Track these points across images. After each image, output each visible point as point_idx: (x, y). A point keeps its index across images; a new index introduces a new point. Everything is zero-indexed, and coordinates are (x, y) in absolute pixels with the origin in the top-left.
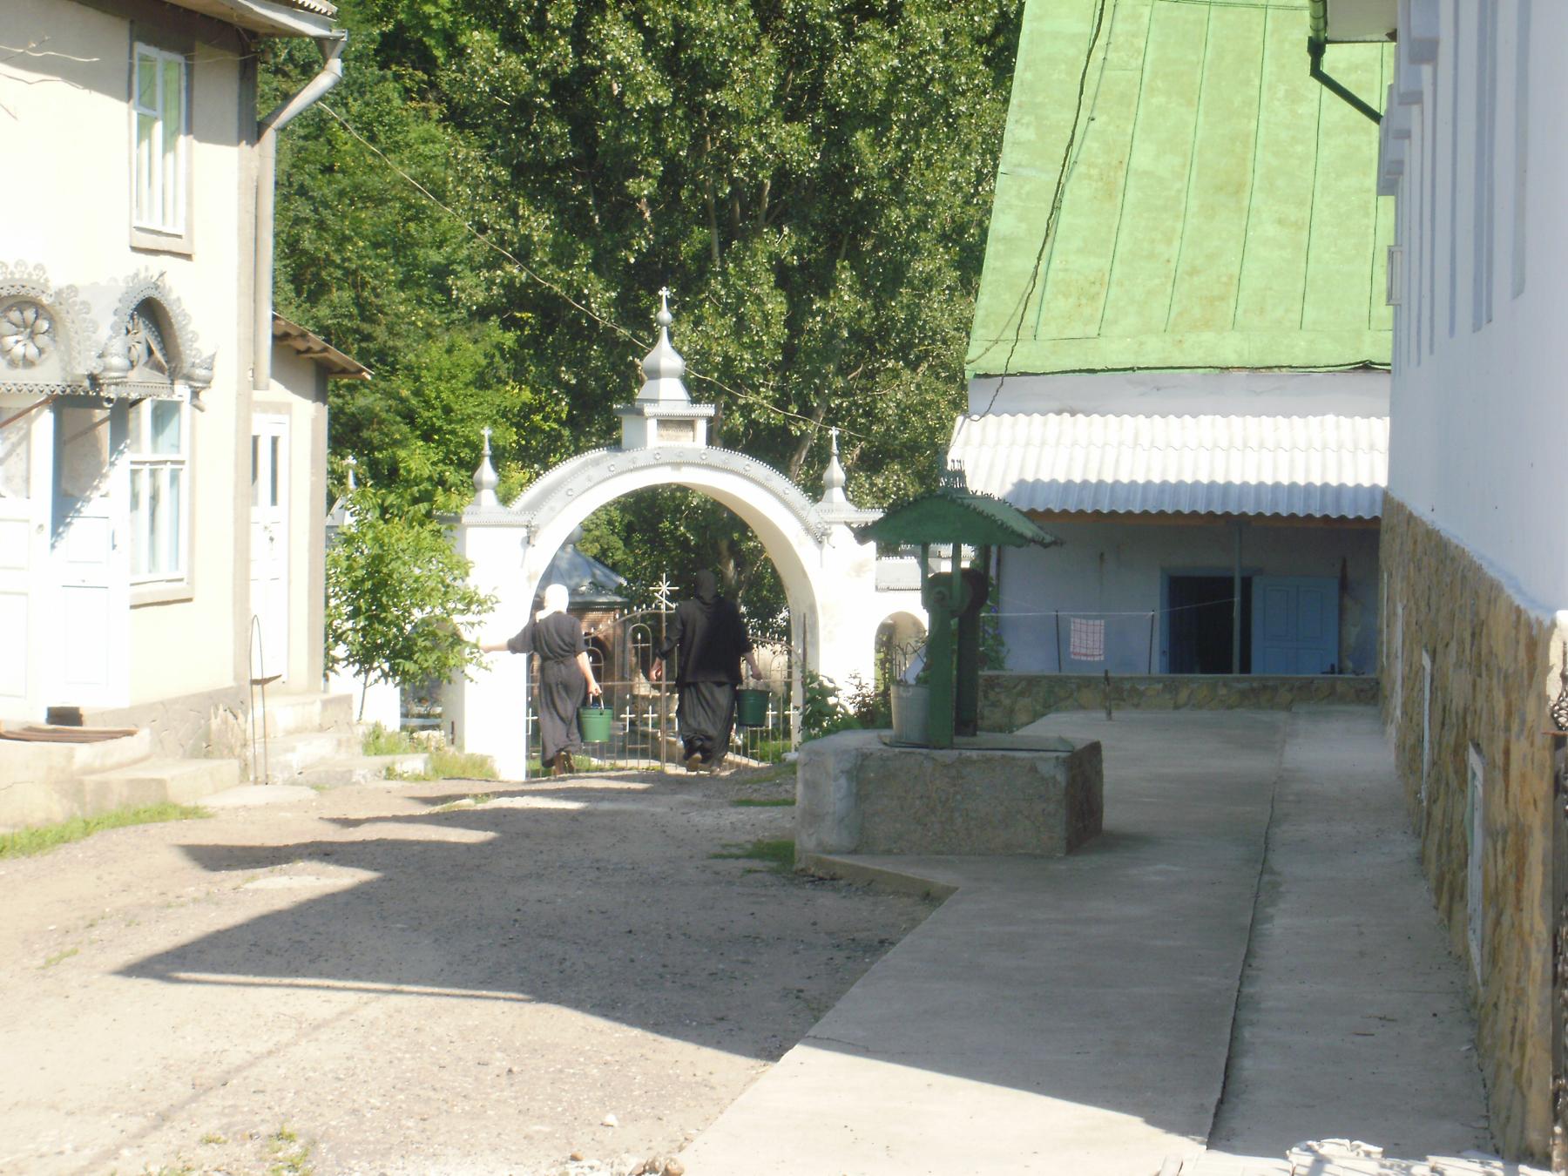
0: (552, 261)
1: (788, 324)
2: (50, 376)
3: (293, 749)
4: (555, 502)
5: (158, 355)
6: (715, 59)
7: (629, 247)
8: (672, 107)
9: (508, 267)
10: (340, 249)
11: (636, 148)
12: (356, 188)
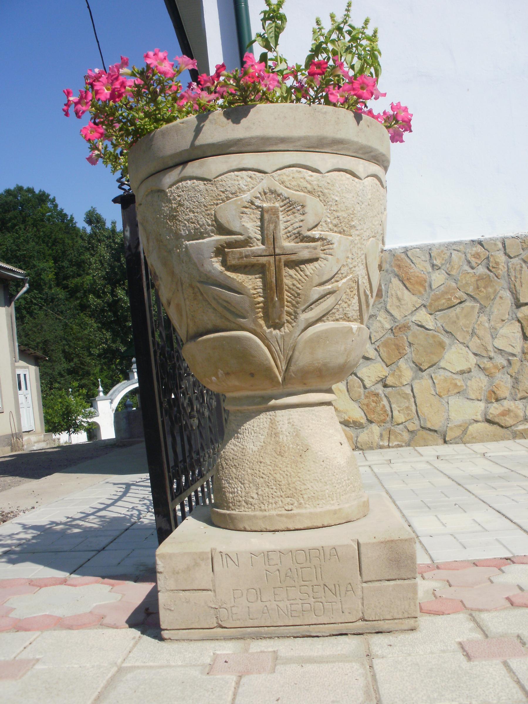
3: (34, 446)
7: (128, 337)
10: (74, 350)
12: (76, 337)
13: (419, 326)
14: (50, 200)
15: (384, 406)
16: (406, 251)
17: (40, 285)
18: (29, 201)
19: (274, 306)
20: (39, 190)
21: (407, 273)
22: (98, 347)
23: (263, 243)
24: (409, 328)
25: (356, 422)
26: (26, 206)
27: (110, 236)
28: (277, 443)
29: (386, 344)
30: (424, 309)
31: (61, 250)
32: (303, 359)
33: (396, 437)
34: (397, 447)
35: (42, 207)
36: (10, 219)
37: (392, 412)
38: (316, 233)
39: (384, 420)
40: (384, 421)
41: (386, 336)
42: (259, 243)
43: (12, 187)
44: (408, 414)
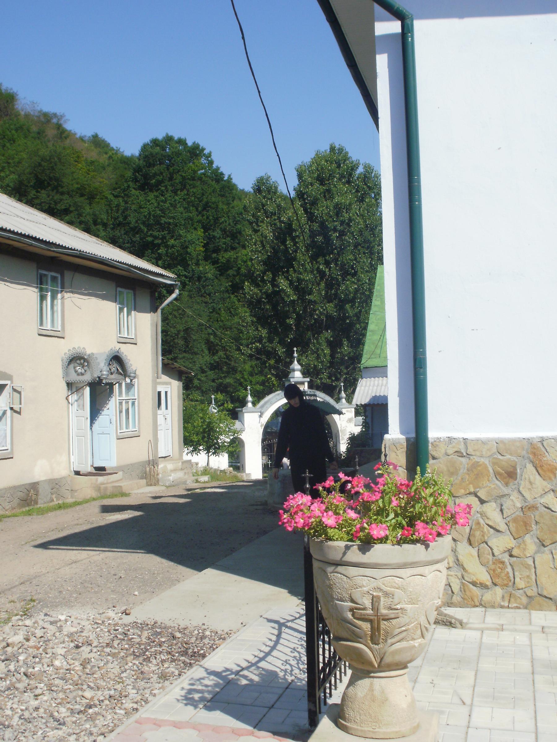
0: (268, 342)
1: (330, 356)
2: (88, 378)
3: (171, 476)
4: (267, 405)
5: (120, 371)
6: (308, 287)
7: (288, 337)
8: (297, 300)
9: (256, 344)
10: (220, 341)
11: (288, 311)
12: (224, 325)
13: (546, 507)
14: (204, 155)
15: (508, 573)
16: (542, 440)
17: (185, 259)
18: (178, 154)
19: (376, 636)
20: (193, 141)
21: (541, 460)
22: (250, 346)
23: (372, 610)
24: (537, 508)
25: (483, 584)
26: (175, 161)
27: (275, 213)
28: (373, 695)
29: (515, 520)
30: (552, 493)
31: (213, 217)
32: (388, 659)
33: (516, 600)
34: (515, 609)
35: (194, 163)
36: (155, 175)
37: (514, 578)
38: (398, 607)
39: (507, 584)
40: (506, 585)
41: (517, 513)
42: (371, 610)
43: (160, 136)
44: (528, 582)
